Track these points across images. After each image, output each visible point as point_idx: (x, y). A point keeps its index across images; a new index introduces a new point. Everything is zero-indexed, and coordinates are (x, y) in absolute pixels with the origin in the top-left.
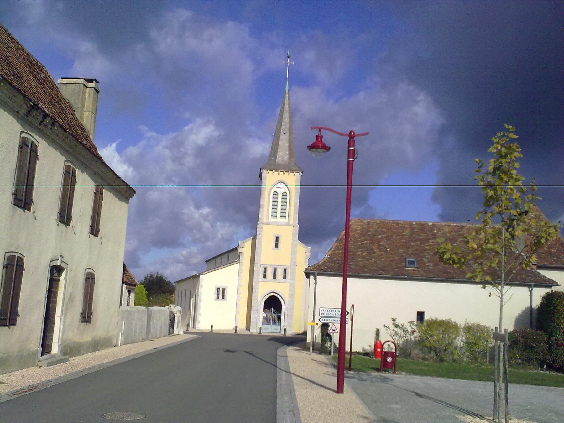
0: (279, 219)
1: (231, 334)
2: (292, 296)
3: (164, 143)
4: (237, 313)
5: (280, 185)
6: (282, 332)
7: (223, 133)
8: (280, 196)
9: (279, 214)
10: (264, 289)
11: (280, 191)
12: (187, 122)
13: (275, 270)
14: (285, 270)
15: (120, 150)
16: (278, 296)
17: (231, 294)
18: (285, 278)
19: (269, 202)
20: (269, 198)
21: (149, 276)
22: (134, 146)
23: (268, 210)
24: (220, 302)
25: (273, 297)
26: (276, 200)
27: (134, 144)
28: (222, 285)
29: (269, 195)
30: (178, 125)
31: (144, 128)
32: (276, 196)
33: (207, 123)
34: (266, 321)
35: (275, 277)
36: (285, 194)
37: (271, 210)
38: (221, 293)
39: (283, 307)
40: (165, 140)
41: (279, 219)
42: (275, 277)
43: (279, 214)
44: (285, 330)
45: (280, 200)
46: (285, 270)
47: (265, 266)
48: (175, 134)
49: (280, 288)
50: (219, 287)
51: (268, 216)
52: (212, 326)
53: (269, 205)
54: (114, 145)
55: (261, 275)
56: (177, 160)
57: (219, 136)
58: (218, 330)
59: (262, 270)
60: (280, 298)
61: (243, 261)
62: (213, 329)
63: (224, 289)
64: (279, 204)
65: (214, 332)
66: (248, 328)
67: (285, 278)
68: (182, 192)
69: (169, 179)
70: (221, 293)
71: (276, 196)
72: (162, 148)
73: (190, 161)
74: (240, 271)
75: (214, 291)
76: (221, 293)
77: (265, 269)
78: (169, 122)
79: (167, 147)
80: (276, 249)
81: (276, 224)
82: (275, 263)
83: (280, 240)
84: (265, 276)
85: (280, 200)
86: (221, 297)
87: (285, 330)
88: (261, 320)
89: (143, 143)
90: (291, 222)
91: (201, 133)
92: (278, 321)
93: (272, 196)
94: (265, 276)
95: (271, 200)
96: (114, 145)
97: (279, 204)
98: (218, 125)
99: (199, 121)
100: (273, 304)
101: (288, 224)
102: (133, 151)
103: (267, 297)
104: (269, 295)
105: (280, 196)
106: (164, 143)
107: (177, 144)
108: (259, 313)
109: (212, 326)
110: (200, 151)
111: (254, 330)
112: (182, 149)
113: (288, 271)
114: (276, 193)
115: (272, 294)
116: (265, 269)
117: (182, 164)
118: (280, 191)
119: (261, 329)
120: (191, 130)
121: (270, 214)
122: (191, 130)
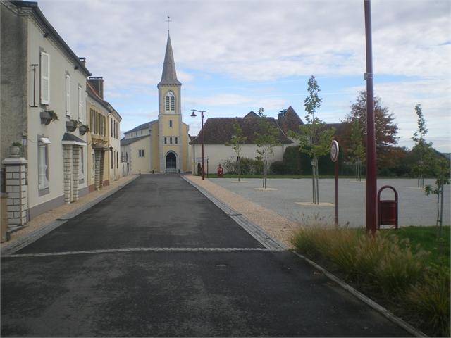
8: (170, 99)
10: (166, 149)
11: (169, 96)
13: (171, 139)
14: (176, 138)
18: (176, 143)
28: (141, 149)
45: (170, 101)
46: (176, 138)
59: (164, 139)
67: (176, 143)
76: (142, 153)
83: (173, 122)
84: (166, 143)
85: (170, 101)
92: (174, 166)
94: (166, 143)
105: (170, 99)
114: (168, 97)
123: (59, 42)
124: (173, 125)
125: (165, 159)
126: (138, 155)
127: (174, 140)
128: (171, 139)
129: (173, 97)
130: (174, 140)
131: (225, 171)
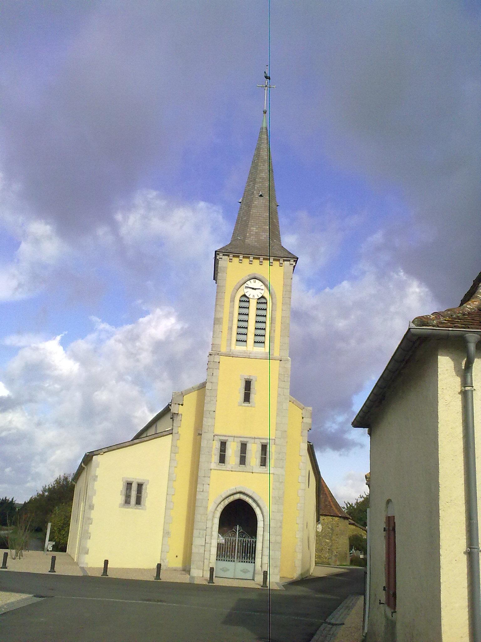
0: (250, 347)
1: (147, 582)
2: (279, 500)
3: (118, 336)
4: (166, 534)
5: (251, 284)
6: (259, 578)
7: (186, 326)
8: (253, 305)
9: (251, 338)
10: (223, 484)
11: (254, 295)
12: (145, 313)
13: (244, 447)
14: (264, 448)
15: (64, 343)
16: (250, 501)
17: (151, 495)
18: (263, 462)
19: (231, 313)
20: (232, 307)
21: (62, 478)
22: (83, 339)
23: (230, 329)
24: (132, 511)
25: (240, 502)
26: (244, 311)
27: (82, 336)
28: (136, 476)
29: (232, 300)
30: (135, 315)
31: (94, 318)
32: (245, 304)
33: (168, 315)
34: (223, 552)
35: (243, 460)
36: (264, 301)
37: (235, 330)
38: (134, 493)
39: (260, 524)
40: (120, 333)
41: (250, 347)
42: (243, 460)
43: (251, 338)
44: (265, 573)
45: (253, 311)
46: (264, 448)
47: (224, 438)
48: (129, 327)
49: (254, 484)
50: (130, 480)
51: (230, 340)
52: (106, 562)
53: (231, 321)
54: (59, 338)
55: (216, 458)
56: (132, 355)
57: (182, 328)
58: (136, 570)
59: (216, 445)
60: (254, 505)
61: (180, 430)
62: (109, 566)
63: (140, 486)
64: (252, 318)
65: (110, 574)
66: (186, 569)
67: (263, 462)
68: (134, 392)
69: (120, 378)
70: (134, 493)
71: (245, 304)
72: (115, 341)
73: (146, 358)
74: (174, 450)
75: (120, 487)
76: (134, 493)
77: (223, 444)
78: (124, 309)
79: (120, 341)
80: (246, 404)
81: (248, 356)
82: (245, 432)
83: (255, 387)
84: (222, 459)
85: (253, 311)
86: (133, 500)
87: (265, 573)
88: (214, 551)
89: (92, 337)
90: (276, 353)
91: (161, 324)
92: (249, 553)
93: (237, 303)
94: (222, 459)
95: (236, 310)
96: (59, 338)
97: (252, 318)
98: (181, 317)
99: (158, 311)
100: (239, 516)
101: (269, 357)
102: (82, 345)
103: (227, 502)
104: (232, 499)
105: (253, 305)
106: (118, 336)
107: (134, 338)
108: (211, 537)
109: (106, 562)
110: (159, 346)
111: (199, 574)
112: (138, 344)
113: (272, 450)
114: (245, 299)
115: (237, 497)
116: (223, 444)
117: (138, 360)
118: (254, 295)
119: (212, 570)
120: (149, 322)
121: (234, 337)
122: (149, 322)
123: (194, 506)
124: (242, 385)
125: (217, 521)
126: (121, 499)
127: (254, 451)
128: (244, 447)
129: (262, 301)
130: (254, 451)
131: (288, 288)
